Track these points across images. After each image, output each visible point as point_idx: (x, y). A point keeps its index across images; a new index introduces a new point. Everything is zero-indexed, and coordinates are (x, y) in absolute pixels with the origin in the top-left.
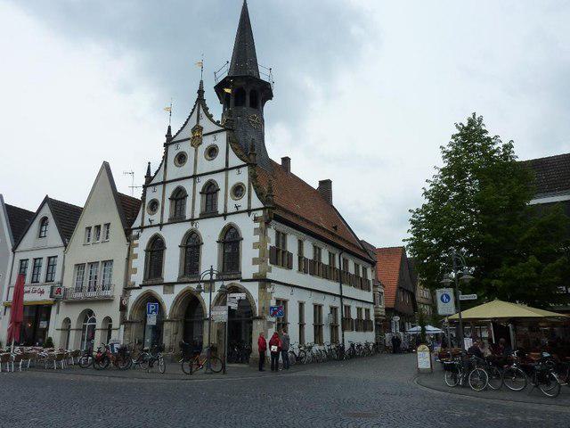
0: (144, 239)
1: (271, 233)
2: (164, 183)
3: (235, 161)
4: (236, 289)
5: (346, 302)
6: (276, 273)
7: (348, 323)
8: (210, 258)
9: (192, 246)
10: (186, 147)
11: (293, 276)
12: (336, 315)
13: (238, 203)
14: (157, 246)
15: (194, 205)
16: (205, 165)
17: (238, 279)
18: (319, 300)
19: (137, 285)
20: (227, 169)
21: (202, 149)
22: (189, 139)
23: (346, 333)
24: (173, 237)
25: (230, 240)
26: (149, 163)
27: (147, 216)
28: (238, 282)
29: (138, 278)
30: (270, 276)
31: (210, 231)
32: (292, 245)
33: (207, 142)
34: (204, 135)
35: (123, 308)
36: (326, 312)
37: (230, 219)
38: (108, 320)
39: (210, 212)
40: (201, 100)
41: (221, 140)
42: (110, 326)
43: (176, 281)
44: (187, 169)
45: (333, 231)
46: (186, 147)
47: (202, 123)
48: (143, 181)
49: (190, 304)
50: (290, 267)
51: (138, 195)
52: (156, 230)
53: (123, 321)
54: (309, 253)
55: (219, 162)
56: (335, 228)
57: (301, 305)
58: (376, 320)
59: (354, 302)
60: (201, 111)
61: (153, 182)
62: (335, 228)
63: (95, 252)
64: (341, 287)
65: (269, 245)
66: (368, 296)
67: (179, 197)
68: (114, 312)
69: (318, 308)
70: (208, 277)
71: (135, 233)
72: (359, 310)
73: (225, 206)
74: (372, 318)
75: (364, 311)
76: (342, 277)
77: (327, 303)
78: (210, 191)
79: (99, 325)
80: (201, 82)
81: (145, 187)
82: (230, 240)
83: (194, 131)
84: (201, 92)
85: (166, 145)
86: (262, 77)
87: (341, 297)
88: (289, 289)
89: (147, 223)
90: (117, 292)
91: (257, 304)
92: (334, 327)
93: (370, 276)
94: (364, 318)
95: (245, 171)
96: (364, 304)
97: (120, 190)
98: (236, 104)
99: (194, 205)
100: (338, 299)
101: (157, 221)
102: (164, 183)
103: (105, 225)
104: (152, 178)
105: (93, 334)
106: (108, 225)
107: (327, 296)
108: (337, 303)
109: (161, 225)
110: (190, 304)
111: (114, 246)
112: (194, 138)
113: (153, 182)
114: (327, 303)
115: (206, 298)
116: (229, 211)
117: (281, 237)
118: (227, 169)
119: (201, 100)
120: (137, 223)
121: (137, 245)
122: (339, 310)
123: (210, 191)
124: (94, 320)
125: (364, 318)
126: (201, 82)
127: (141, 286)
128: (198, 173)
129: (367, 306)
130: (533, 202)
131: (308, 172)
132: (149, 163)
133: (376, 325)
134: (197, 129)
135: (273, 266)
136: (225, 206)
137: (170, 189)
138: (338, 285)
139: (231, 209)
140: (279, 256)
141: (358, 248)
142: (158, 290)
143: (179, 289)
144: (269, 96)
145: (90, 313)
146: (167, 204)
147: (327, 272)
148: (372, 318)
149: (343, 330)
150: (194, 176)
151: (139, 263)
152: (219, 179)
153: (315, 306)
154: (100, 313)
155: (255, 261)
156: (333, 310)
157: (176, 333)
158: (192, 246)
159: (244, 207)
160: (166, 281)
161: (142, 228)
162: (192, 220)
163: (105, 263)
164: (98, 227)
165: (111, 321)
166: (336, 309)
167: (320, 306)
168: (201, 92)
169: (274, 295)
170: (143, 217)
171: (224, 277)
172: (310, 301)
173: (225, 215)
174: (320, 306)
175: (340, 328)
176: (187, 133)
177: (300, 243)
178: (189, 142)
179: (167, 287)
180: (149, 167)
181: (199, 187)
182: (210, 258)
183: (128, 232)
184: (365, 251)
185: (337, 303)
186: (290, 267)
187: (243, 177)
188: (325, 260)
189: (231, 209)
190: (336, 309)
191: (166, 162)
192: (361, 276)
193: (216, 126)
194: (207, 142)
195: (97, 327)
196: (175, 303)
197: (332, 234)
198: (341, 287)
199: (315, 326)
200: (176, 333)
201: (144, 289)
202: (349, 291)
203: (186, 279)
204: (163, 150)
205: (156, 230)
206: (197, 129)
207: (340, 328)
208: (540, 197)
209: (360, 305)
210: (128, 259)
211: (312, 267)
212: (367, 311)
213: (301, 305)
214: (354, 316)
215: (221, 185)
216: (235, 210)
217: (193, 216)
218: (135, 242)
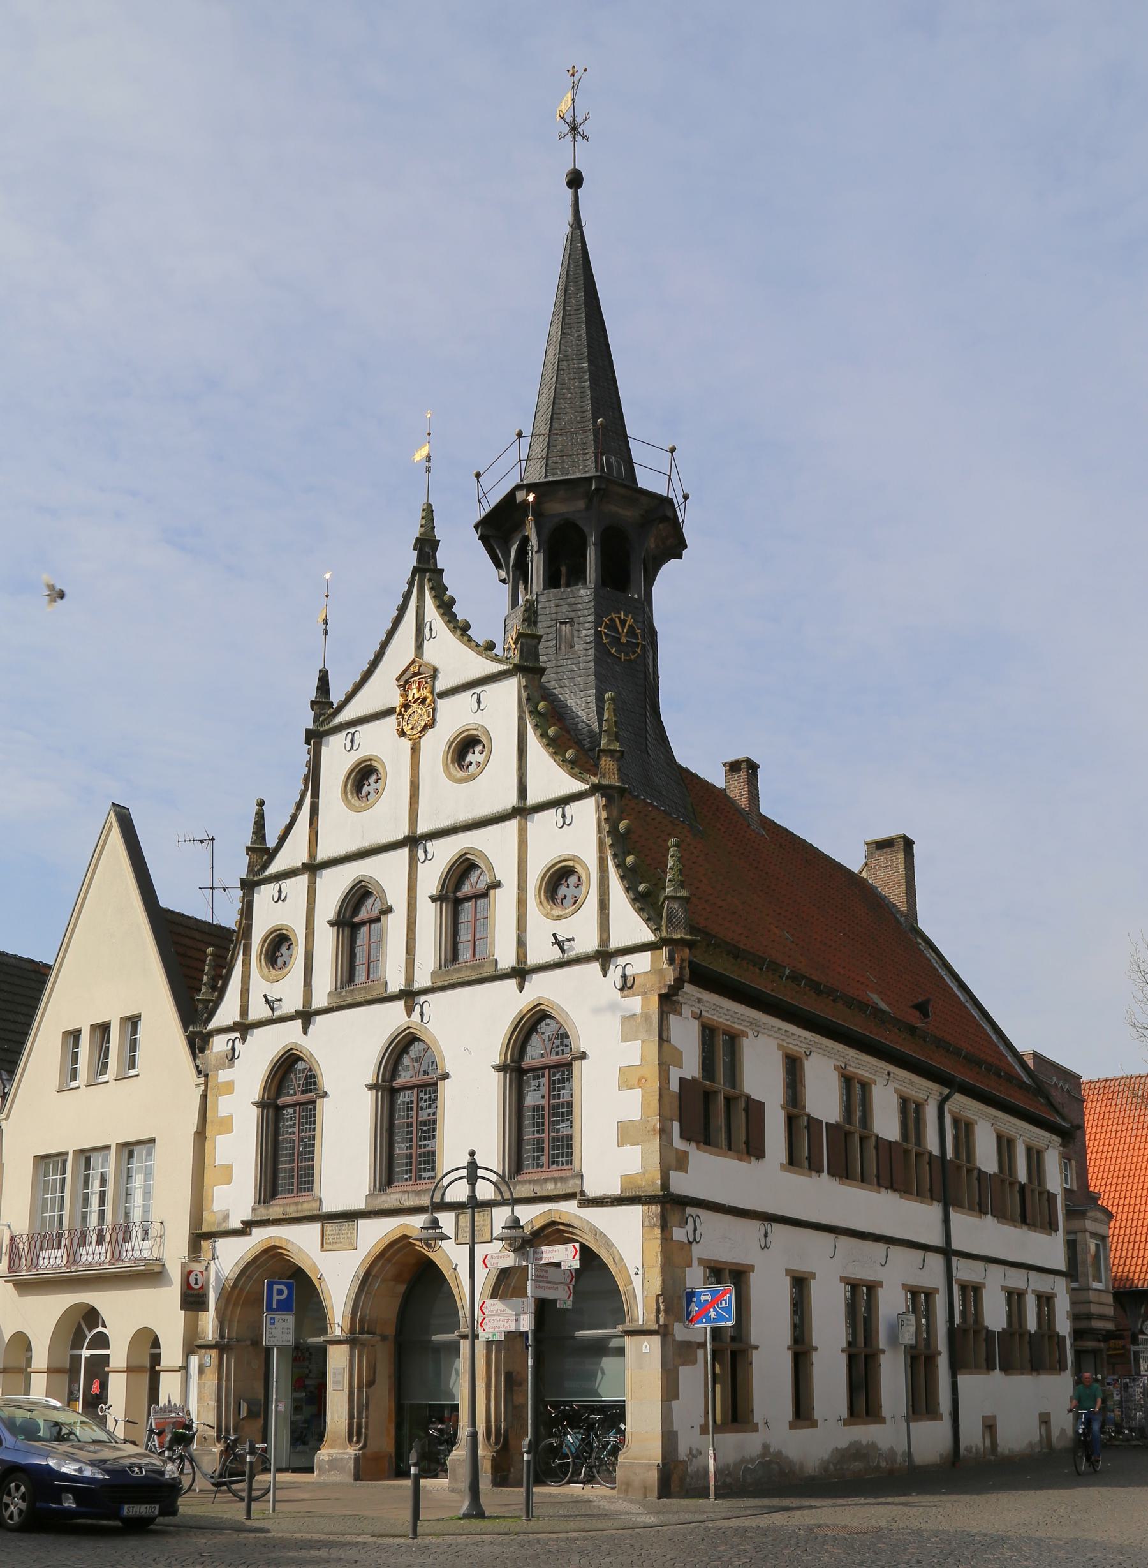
0: (259, 1054)
1: (686, 1034)
2: (313, 868)
3: (550, 776)
4: (553, 1232)
5: (965, 1271)
6: (710, 1174)
7: (972, 1346)
8: (471, 1122)
9: (406, 1087)
10: (381, 742)
11: (766, 1180)
12: (929, 1314)
13: (564, 929)
14: (290, 1092)
15: (408, 944)
16: (447, 799)
17: (570, 1196)
18: (867, 1263)
19: (235, 1224)
20: (522, 811)
21: (436, 745)
22: (389, 712)
23: (963, 1380)
24: (347, 1054)
25: (537, 1064)
26: (261, 803)
27: (259, 985)
28: (568, 1210)
29: (235, 1198)
30: (681, 1184)
31: (469, 1033)
32: (760, 1076)
33: (455, 716)
34: (443, 695)
35: (193, 1300)
36: (891, 1303)
37: (540, 988)
38: (148, 1343)
39: (463, 963)
40: (426, 567)
41: (501, 709)
42: (156, 1359)
43: (360, 1204)
44: (386, 817)
45: (915, 1019)
46: (381, 742)
47: (432, 654)
48: (240, 867)
49: (411, 1287)
50: (754, 1149)
51: (227, 917)
52: (289, 1035)
53: (192, 1346)
54: (824, 1102)
55: (494, 788)
56: (922, 1008)
57: (800, 1283)
58: (1078, 1334)
59: (996, 1270)
60: (431, 612)
61: (273, 869)
62: (922, 1008)
63: (93, 1115)
64: (946, 1221)
65: (675, 1074)
66: (1049, 1249)
67: (357, 914)
68: (160, 1310)
69: (861, 1298)
70: (458, 1192)
71: (219, 1044)
72: (1015, 1298)
73: (521, 944)
74: (1063, 1326)
75: (1031, 1303)
76: (947, 1182)
77: (895, 1276)
78: (462, 888)
79: (118, 1355)
80: (429, 511)
81: (249, 886)
82: (537, 1064)
83: (404, 682)
84: (427, 546)
85: (315, 738)
86: (646, 480)
87: (947, 1252)
88: (754, 1228)
89: (258, 1011)
90: (174, 1252)
91: (637, 1282)
92: (920, 1361)
93: (1055, 1181)
94: (1032, 1325)
95: (587, 813)
96: (1033, 1275)
97: (166, 901)
98: (552, 581)
99: (408, 944)
100: (936, 1262)
101: (292, 1002)
102: (313, 868)
103: (94, 1027)
104: (272, 854)
105: (104, 1386)
106: (132, 1022)
107: (896, 1252)
108: (932, 1273)
109: (306, 1016)
110: (411, 1287)
111: (155, 1093)
112: (406, 706)
113: (274, 868)
114: (895, 1276)
115: (452, 1255)
116: (533, 959)
117: (719, 1047)
118: (522, 811)
119: (426, 567)
120: (227, 1013)
121: (229, 1087)
122: (940, 1301)
123: (462, 888)
124: (102, 1341)
125: (1032, 1325)
126: (429, 511)
127: (247, 1227)
128: (423, 828)
129: (1043, 1283)
130: (581, 1333)
131: (828, 812)
132: (261, 803)
133: (1078, 1354)
134: (417, 675)
135: (691, 1149)
136: (521, 944)
137: (333, 887)
138: (934, 1211)
139: (540, 951)
140: (704, 1111)
141: (1022, 1085)
142: (303, 1242)
143: (374, 1234)
144: (675, 546)
145: (91, 1316)
146: (326, 941)
147: (895, 1168)
148: (1063, 1326)
149: (955, 1368)
150: (413, 841)
151: (239, 1147)
152: (496, 847)
153: (854, 1286)
154: (124, 1314)
155: (626, 1134)
156: (920, 1298)
157: (371, 1383)
158: (406, 1087)
159: (588, 943)
160: (327, 1208)
161: (243, 1028)
162: (409, 996)
163: (128, 1149)
164: (103, 1029)
165: (156, 1343)
166: (929, 1294)
167: (872, 1287)
168: (427, 546)
169: (697, 1251)
170: (250, 988)
171: (522, 1191)
172: (830, 1270)
173: (521, 973)
174: (872, 1287)
175: (943, 1362)
176: (382, 691)
177: (793, 1067)
178: (392, 720)
179: (330, 1227)
180: (260, 816)
181: (431, 877)
182: (471, 1122)
183: (198, 1043)
184: (1039, 1090)
185: (932, 1273)
186: (754, 1149)
187: (579, 835)
188: (886, 1124)
189: (540, 951)
190: (929, 1294)
191: (315, 795)
192: (1022, 1176)
193: (481, 660)
194: (455, 716)
195: (113, 1364)
196: (367, 1280)
197: (912, 1030)
198: (946, 1221)
199: (851, 1360)
200: (371, 1383)
201: (261, 1236)
202: (976, 1232)
203: (392, 1199)
204: (303, 753)
205: (289, 1035)
206: (417, 675)
207: (943, 1362)
208: (792, 1499)
209: (1017, 1280)
210: (201, 1135)
211: (836, 1150)
212: (1046, 1300)
213: (800, 1283)
214: (995, 1317)
215: (505, 869)
216: (555, 954)
217: (409, 979)
218: (223, 1076)
